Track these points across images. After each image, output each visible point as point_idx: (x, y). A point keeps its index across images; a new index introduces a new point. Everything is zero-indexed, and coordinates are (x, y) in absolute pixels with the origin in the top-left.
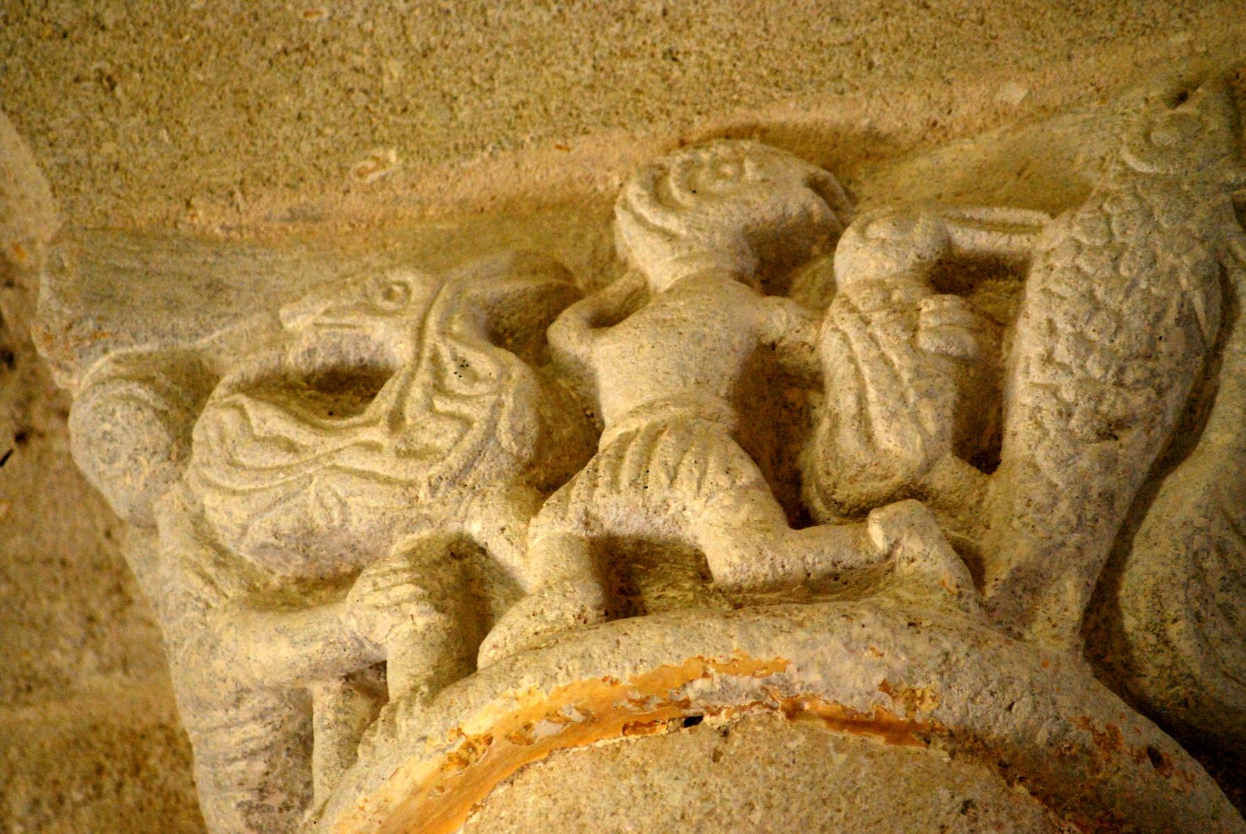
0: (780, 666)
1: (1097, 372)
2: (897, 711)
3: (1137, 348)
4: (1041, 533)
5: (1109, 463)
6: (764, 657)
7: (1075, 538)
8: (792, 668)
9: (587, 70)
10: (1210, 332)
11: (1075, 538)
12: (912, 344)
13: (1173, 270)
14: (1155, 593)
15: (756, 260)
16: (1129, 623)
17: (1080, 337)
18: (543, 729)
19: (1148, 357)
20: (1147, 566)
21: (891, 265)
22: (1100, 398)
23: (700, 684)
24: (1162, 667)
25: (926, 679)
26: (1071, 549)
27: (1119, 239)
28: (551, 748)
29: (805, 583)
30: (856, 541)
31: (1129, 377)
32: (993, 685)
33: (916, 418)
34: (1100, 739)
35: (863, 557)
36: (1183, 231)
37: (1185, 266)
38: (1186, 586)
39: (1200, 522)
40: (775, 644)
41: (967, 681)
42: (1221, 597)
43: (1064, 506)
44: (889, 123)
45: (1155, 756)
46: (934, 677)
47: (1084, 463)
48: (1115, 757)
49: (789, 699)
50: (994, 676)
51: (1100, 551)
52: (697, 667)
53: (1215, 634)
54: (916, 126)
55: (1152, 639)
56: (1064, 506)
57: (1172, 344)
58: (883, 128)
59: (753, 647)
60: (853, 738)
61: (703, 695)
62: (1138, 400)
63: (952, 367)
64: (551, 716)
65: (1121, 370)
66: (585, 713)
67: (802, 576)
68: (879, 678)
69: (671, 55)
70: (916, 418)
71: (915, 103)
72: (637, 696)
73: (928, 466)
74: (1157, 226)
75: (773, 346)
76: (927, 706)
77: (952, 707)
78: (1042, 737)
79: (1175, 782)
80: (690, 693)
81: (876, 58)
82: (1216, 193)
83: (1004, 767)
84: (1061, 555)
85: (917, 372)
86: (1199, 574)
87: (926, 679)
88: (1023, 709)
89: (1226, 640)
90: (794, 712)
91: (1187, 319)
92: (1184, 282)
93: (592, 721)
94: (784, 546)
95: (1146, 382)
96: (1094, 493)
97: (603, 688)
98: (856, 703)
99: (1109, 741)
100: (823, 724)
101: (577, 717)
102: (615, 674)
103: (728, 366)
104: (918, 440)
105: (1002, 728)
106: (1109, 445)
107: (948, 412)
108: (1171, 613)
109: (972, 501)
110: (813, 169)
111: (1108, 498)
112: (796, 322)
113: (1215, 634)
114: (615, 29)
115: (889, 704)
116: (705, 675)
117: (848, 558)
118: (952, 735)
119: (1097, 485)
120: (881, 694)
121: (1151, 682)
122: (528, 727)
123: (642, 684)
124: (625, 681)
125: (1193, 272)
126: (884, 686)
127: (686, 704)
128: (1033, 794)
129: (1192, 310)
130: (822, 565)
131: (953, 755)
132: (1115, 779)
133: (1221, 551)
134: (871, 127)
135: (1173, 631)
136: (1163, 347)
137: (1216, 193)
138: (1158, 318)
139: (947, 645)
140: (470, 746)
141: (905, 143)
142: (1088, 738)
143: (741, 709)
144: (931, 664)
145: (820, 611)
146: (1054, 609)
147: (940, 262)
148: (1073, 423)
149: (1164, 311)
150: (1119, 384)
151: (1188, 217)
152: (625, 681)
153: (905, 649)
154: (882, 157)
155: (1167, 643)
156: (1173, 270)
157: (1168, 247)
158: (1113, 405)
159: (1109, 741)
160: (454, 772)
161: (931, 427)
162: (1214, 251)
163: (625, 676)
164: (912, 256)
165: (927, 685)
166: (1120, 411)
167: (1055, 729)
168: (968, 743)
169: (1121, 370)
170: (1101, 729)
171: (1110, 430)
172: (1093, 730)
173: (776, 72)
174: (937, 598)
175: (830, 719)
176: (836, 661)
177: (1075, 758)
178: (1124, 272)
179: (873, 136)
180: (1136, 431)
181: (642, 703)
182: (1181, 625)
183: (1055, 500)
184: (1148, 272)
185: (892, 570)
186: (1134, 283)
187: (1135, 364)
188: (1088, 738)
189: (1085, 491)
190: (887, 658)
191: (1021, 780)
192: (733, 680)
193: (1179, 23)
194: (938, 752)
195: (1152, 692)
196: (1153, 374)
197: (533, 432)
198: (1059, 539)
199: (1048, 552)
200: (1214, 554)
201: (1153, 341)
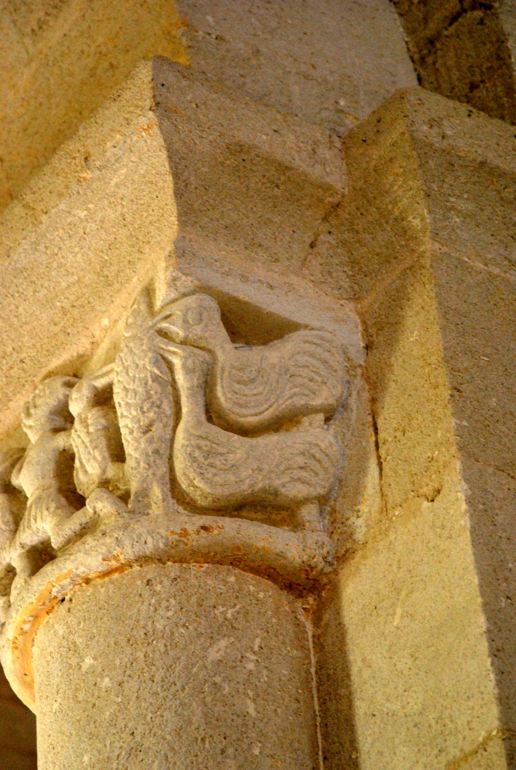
0: (71, 571)
1: (134, 413)
2: (114, 564)
3: (143, 398)
4: (139, 476)
5: (150, 441)
6: (65, 571)
7: (150, 472)
8: (74, 570)
9: (4, 379)
10: (167, 378)
11: (150, 472)
12: (88, 433)
13: (144, 365)
14: (184, 474)
15: (62, 419)
16: (184, 486)
17: (127, 404)
18: (26, 627)
19: (149, 398)
20: (179, 466)
21: (81, 406)
22: (139, 421)
23: (54, 590)
24: (200, 495)
25: (115, 550)
26: (151, 476)
27: (126, 364)
28: (34, 630)
29: (76, 535)
30: (85, 513)
31: (145, 409)
32: (136, 539)
33: (95, 458)
34: (180, 535)
35: (88, 517)
36: (142, 351)
37: (146, 362)
38: (192, 466)
39: (186, 443)
40: (66, 565)
41: (127, 543)
42: (206, 462)
43: (142, 464)
44: (81, 350)
45: (205, 528)
46: (117, 548)
47: (143, 446)
48: (189, 537)
49: (82, 579)
50: (135, 536)
51: (164, 469)
52: (50, 586)
53: (210, 476)
54: (88, 346)
55: (192, 488)
56: (142, 464)
57: (155, 388)
58: (81, 352)
59: (61, 570)
60: (107, 579)
61: (58, 592)
62: (151, 415)
63: (102, 433)
64: (25, 622)
65: (142, 408)
66: (32, 616)
67: (73, 534)
68: (100, 558)
69: (22, 361)
70: (95, 458)
71: (83, 340)
72: (41, 603)
73: (104, 471)
74: (135, 354)
75: (64, 450)
76: (122, 557)
77: (128, 552)
78: (161, 545)
79: (216, 532)
80: (54, 593)
81: (69, 331)
82: (148, 332)
83: (160, 560)
84: (149, 480)
85: (91, 442)
86: (195, 460)
87: (115, 550)
88: (150, 540)
89: (215, 475)
90: (87, 581)
91: (156, 379)
92: (149, 368)
93: (36, 617)
94: (64, 528)
95: (151, 407)
96: (150, 453)
97: (31, 607)
98: (100, 569)
99: (185, 533)
100: (98, 579)
101: (31, 619)
102: (31, 600)
103: (51, 467)
104: (97, 465)
105: (149, 549)
106: (148, 435)
107: (105, 449)
108: (192, 478)
109: (121, 476)
110: (67, 378)
111: (157, 452)
112: (65, 438)
113: (210, 476)
114: (4, 362)
115: (110, 563)
116: (53, 586)
117: (84, 520)
118: (136, 560)
119: (150, 451)
120: (105, 563)
121: (201, 502)
122: (22, 629)
123: (39, 600)
124: (35, 601)
125: (150, 363)
126: (104, 560)
127: (56, 597)
128: (174, 562)
129: (156, 375)
130: (78, 528)
131: (141, 566)
132: (194, 544)
133: (199, 448)
134: (78, 353)
135: (196, 482)
136: (152, 392)
137: (148, 332)
138: (146, 384)
139: (116, 535)
140: (14, 643)
141: (88, 353)
142: (176, 537)
143: (71, 590)
144: (113, 545)
145: (89, 539)
146: (155, 498)
147: (95, 395)
148: (135, 434)
149: (147, 380)
150: (143, 412)
151: (142, 345)
152: (35, 601)
153: (103, 544)
154: (86, 361)
155: (197, 487)
156: (144, 365)
157: (139, 359)
158: (144, 422)
159: (185, 533)
160: (16, 652)
161: (99, 458)
162: (154, 351)
163: (33, 600)
164: (85, 399)
165: (117, 551)
166: (147, 421)
167: (164, 541)
168: (143, 560)
169: (142, 408)
170: (179, 532)
171: (147, 430)
172: (176, 533)
173: (48, 351)
174: (113, 518)
175: (99, 577)
176: (87, 560)
177: (177, 546)
178: (131, 375)
179: (80, 356)
180: (156, 424)
181: (44, 604)
182: (197, 480)
183: (138, 463)
184: (137, 370)
185: (99, 516)
186: (134, 376)
187: (145, 403)
188: (176, 537)
189: (147, 455)
190: (99, 551)
191: (168, 560)
192: (62, 583)
193: (133, 274)
194: (136, 568)
195: (203, 504)
196: (153, 403)
197: (11, 519)
198: (145, 475)
199: (144, 481)
200: (197, 451)
201: (148, 392)
